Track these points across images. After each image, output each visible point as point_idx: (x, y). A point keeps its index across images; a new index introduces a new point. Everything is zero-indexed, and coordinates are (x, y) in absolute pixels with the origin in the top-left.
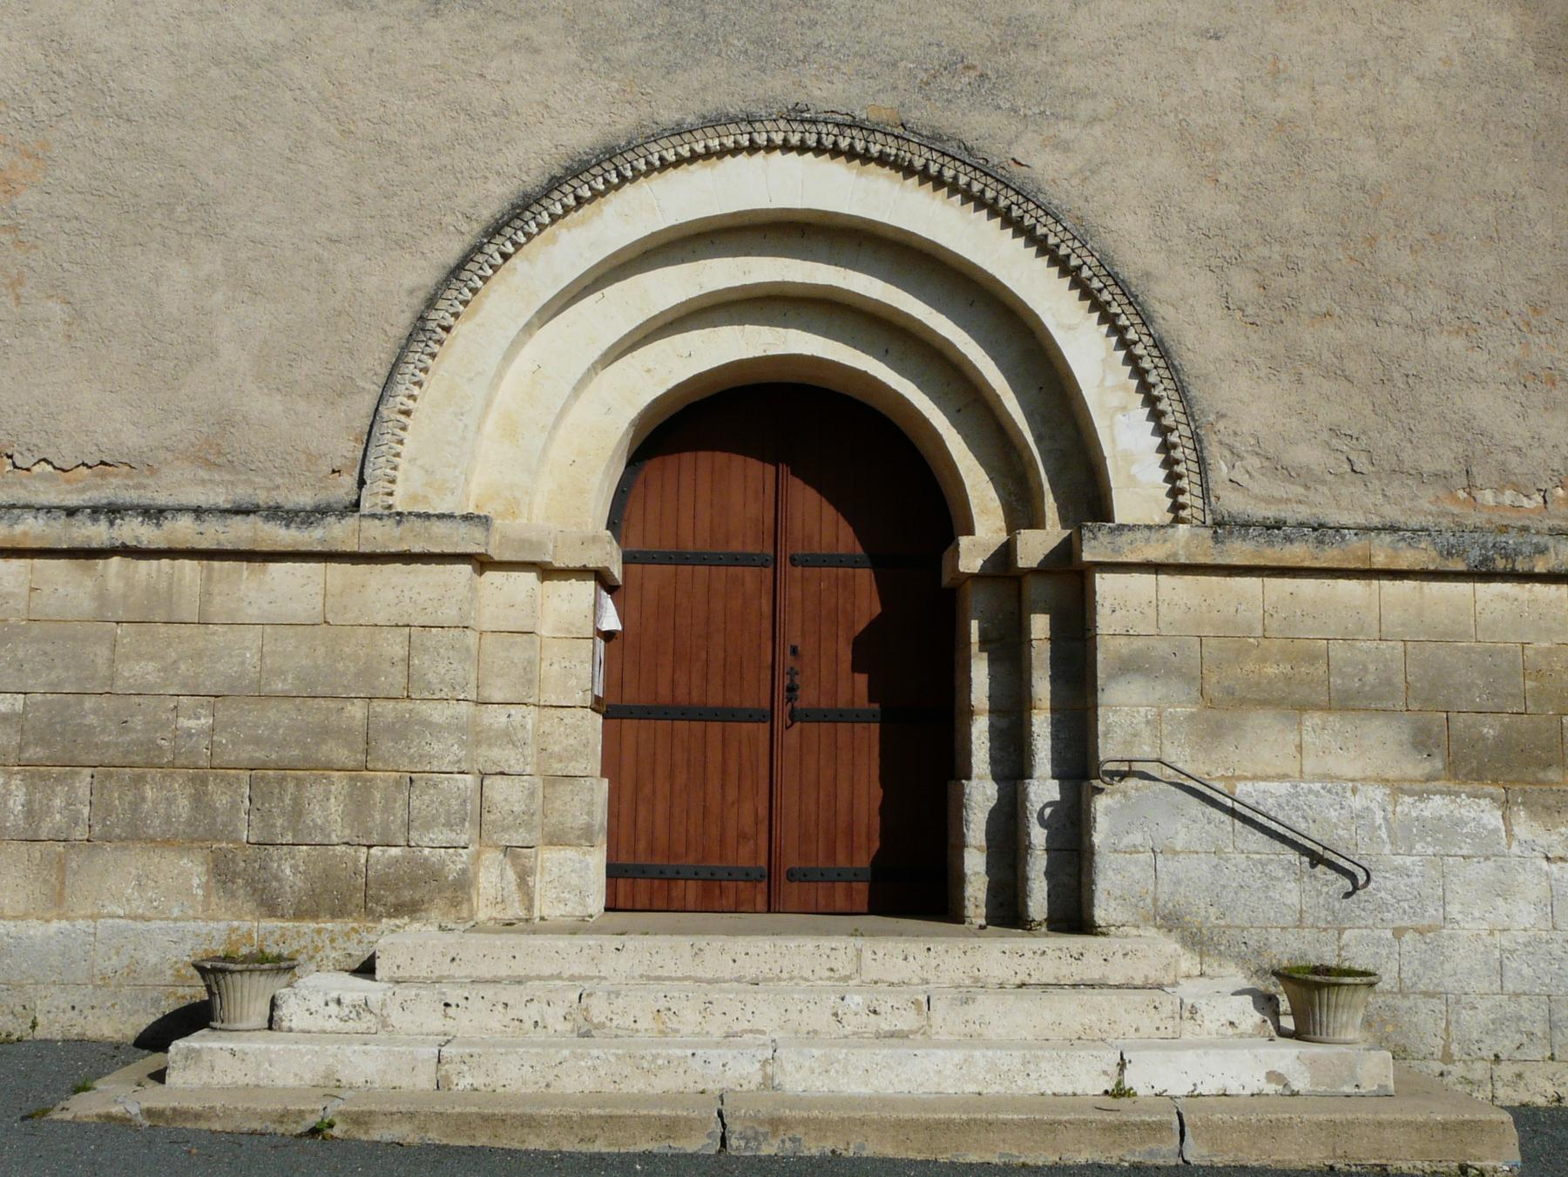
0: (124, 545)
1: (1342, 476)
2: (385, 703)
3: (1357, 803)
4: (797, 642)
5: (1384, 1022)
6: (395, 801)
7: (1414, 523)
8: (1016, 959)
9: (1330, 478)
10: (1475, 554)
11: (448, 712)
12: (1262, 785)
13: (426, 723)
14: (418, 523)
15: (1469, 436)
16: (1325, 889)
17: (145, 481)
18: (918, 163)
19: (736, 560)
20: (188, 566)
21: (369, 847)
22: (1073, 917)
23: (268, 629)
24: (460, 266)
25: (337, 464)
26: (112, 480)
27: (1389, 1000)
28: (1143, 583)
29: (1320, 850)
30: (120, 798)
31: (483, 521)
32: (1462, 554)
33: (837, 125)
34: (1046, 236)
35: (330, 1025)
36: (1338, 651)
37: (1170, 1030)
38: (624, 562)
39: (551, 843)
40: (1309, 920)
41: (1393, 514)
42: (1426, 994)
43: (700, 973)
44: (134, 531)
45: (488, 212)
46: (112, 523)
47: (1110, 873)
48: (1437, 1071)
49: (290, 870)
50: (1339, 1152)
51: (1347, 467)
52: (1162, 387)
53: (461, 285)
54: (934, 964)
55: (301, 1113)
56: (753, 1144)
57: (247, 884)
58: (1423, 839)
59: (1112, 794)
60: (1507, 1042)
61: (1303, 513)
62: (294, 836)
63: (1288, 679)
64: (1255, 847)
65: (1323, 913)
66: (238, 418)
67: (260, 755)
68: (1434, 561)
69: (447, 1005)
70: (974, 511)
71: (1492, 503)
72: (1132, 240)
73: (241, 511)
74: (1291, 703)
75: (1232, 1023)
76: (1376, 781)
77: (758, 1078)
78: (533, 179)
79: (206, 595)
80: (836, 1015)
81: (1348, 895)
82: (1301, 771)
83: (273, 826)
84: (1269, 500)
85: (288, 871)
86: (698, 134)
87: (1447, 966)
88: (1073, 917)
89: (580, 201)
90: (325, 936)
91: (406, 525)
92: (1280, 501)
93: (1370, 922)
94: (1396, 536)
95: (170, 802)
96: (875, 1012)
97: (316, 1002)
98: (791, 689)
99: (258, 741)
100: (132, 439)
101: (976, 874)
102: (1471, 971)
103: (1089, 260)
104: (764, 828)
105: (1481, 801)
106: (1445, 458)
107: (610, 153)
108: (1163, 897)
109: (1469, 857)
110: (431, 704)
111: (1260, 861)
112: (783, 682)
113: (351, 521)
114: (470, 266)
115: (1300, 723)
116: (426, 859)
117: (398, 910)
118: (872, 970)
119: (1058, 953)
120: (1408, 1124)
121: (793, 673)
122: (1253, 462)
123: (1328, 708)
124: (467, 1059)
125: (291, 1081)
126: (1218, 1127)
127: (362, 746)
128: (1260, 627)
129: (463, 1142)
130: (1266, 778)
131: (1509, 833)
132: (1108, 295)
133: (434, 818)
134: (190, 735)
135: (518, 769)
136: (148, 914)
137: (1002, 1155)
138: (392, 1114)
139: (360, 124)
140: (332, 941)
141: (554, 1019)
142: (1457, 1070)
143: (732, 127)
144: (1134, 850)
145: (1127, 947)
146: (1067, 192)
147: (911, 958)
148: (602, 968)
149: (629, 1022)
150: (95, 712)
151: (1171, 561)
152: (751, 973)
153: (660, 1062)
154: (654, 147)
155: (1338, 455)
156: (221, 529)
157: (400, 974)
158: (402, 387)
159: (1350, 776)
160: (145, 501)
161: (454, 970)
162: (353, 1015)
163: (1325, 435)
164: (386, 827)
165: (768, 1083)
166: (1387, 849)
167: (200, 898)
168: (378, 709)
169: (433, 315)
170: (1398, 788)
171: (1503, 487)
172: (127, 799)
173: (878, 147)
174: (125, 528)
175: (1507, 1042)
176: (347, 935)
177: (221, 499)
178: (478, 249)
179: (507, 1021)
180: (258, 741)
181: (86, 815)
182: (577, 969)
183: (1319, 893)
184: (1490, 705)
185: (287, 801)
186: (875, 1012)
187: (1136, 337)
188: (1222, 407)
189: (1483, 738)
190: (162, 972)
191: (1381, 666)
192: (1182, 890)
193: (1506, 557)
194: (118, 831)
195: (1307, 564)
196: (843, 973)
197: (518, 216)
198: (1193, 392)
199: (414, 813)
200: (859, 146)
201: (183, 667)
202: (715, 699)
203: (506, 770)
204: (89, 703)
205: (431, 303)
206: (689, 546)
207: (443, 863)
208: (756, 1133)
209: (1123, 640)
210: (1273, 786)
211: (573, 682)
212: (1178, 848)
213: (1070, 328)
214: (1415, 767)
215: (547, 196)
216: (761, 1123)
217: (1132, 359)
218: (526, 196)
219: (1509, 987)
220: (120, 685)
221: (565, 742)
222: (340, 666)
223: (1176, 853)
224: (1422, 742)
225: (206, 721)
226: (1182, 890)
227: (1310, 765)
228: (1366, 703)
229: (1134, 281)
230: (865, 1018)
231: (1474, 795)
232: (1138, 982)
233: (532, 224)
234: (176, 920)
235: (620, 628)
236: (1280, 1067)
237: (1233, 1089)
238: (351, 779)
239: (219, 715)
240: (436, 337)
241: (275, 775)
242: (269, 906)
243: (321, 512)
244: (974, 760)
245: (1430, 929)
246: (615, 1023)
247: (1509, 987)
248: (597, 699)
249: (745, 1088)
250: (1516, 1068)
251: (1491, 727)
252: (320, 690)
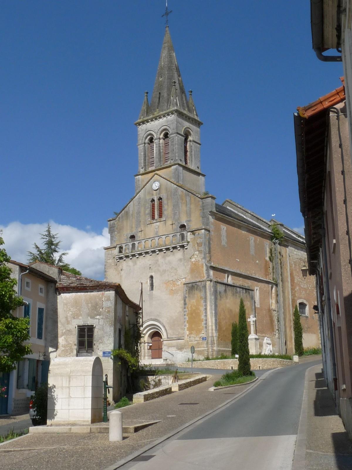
28: (165, 341)
106: (177, 333)
132: (164, 327)
170: (175, 351)
214: (176, 350)
224: (177, 348)
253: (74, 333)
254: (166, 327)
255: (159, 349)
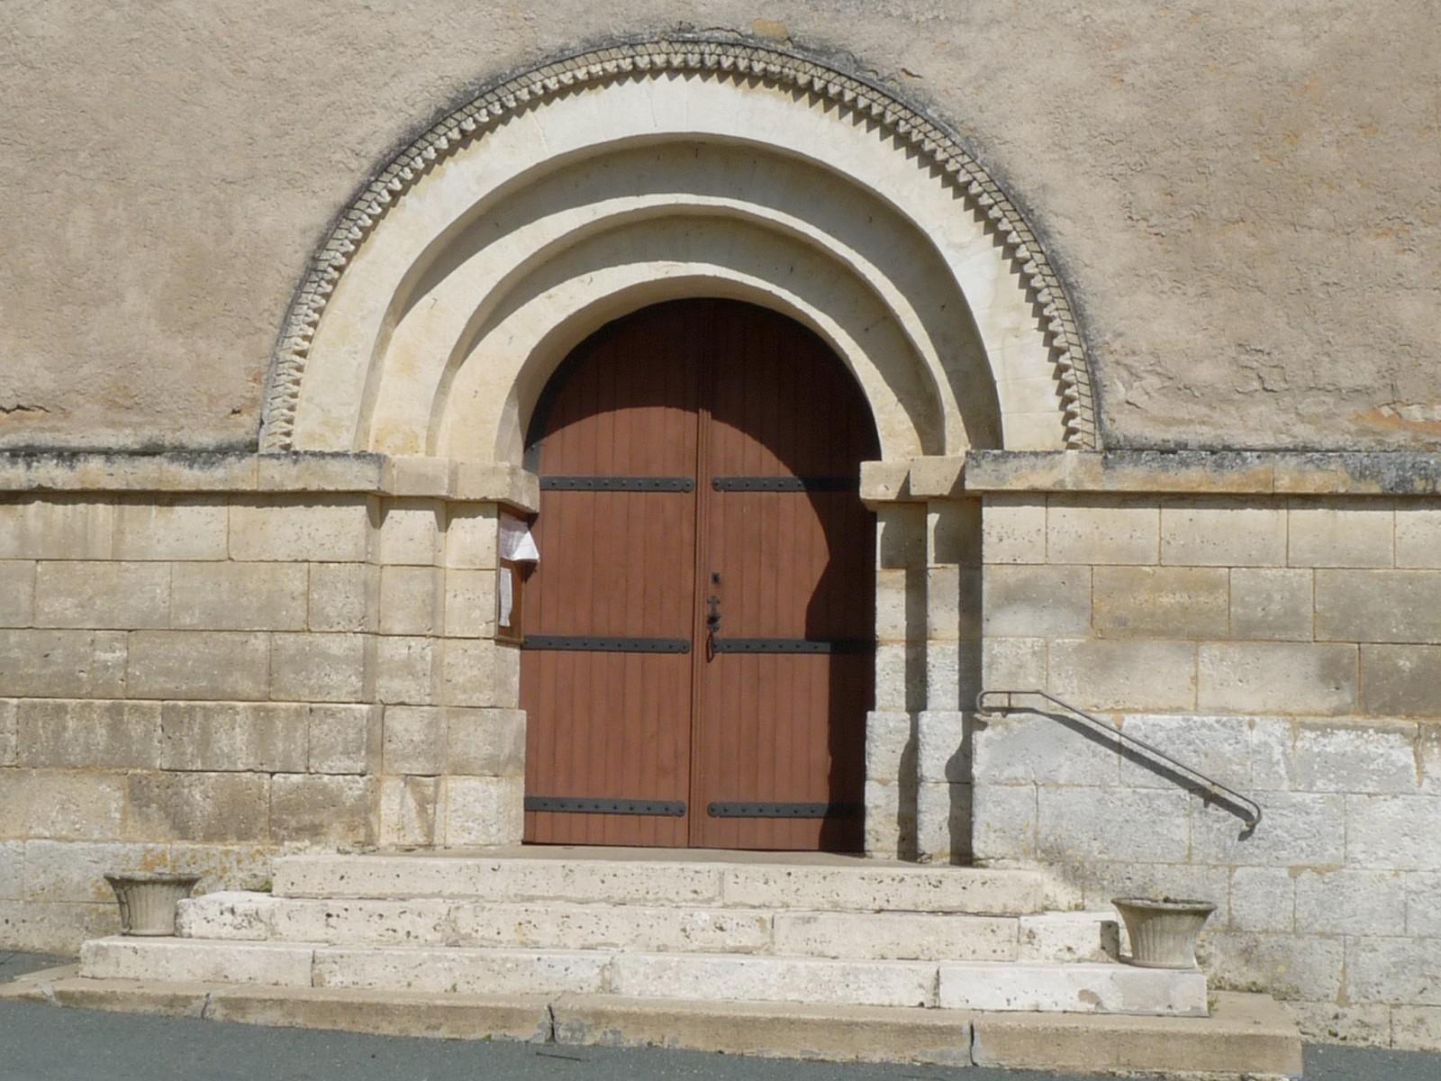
0: (40, 487)
1: (1250, 394)
2: (286, 635)
3: (1254, 737)
4: (718, 570)
5: (1275, 963)
6: (296, 729)
7: (1328, 443)
8: (875, 885)
9: (1237, 396)
10: (1391, 476)
11: (346, 645)
12: (1152, 718)
13: (325, 656)
14: (313, 462)
15: (1395, 347)
16: (1217, 826)
17: (60, 425)
18: (803, 79)
19: (656, 486)
20: (102, 510)
21: (272, 774)
22: (963, 855)
23: (176, 565)
24: (350, 206)
25: (237, 405)
26: (29, 423)
27: (1282, 940)
28: (1031, 515)
29: (1207, 784)
30: (44, 727)
31: (379, 460)
32: (1377, 476)
33: (720, 44)
34: (934, 151)
35: (225, 932)
36: (1240, 578)
37: (1007, 953)
38: (541, 490)
39: (455, 773)
40: (1196, 859)
41: (1304, 433)
42: (1322, 935)
43: (570, 893)
44: (51, 473)
45: (376, 148)
46: (29, 466)
47: (990, 805)
48: (1332, 1014)
49: (200, 797)
50: (1123, 1060)
51: (1256, 385)
52: (1053, 306)
53: (351, 224)
54: (794, 888)
55: (188, 999)
56: (578, 1035)
57: (160, 808)
58: (1324, 775)
59: (995, 725)
60: (1409, 986)
61: (1206, 434)
62: (203, 764)
63: (1184, 609)
64: (1142, 781)
65: (1214, 850)
66: (144, 360)
67: (171, 686)
68: (1344, 483)
69: (329, 915)
70: (881, 434)
71: (1421, 420)
72: (1029, 154)
73: (151, 451)
74: (1188, 632)
75: (1069, 949)
76: (1277, 714)
77: (597, 982)
78: (420, 113)
79: (119, 532)
80: (684, 930)
81: (1244, 836)
82: (1196, 704)
83: (184, 753)
84: (1170, 422)
85: (198, 797)
86: (580, 61)
87: (1346, 907)
88: (963, 855)
89: (395, 195)
90: (233, 858)
91: (302, 464)
92: (1181, 422)
93: (1264, 860)
94: (1303, 458)
95: (89, 730)
96: (721, 929)
97: (213, 911)
98: (712, 620)
99: (168, 673)
100: (46, 382)
101: (877, 807)
102: (1372, 912)
103: (979, 176)
104: (685, 760)
105: (1391, 737)
106: (1360, 370)
107: (493, 84)
108: (1044, 831)
109: (1375, 795)
110: (330, 637)
111: (1147, 795)
112: (704, 612)
113: (250, 461)
114: (360, 205)
115: (1196, 654)
116: (325, 786)
117: (300, 832)
118: (734, 893)
119: (917, 881)
120: (1191, 1036)
121: (714, 602)
122: (1153, 382)
123: (1226, 639)
124: (338, 959)
125: (186, 977)
126: (1006, 1033)
127: (265, 678)
128: (1156, 554)
129: (327, 1026)
130: (1159, 711)
131: (1421, 772)
132: (1003, 210)
133: (332, 747)
134: (107, 668)
135: (416, 700)
136: (72, 836)
137: (803, 1052)
138: (266, 1001)
139: (252, 62)
140: (239, 862)
141: (423, 927)
142: (1354, 1013)
143: (614, 52)
144: (1015, 782)
145: (1011, 878)
146: (960, 102)
147: (771, 883)
148: (480, 887)
149: (493, 934)
150: (20, 645)
151: (1058, 488)
152: (618, 895)
153: (509, 965)
154: (536, 76)
155: (1247, 372)
156: (129, 470)
157: (294, 890)
158: (299, 328)
159: (1250, 709)
160: (57, 444)
161: (342, 887)
162: (245, 924)
163: (1232, 352)
164: (287, 756)
165: (606, 987)
166: (1285, 786)
167: (118, 822)
168: (280, 642)
169: (325, 255)
170: (1298, 724)
171: (1432, 401)
172: (51, 728)
173: (762, 65)
174: (41, 470)
175: (1409, 986)
176: (253, 856)
177: (128, 439)
178: (367, 187)
179: (382, 931)
180: (168, 673)
181: (14, 743)
182: (455, 888)
183: (1210, 829)
184: (1407, 635)
185: (196, 730)
186: (721, 929)
187: (1027, 254)
188: (1120, 326)
189: (1399, 670)
190: (85, 890)
191: (1287, 594)
192: (1064, 823)
193: (1426, 478)
194: (43, 758)
195: (1203, 489)
196: (707, 895)
197: (403, 153)
198: (1090, 310)
199: (314, 741)
200: (742, 65)
201: (98, 602)
202: (635, 629)
203: (407, 701)
204: (14, 637)
205: (323, 244)
206: (609, 473)
207: (341, 790)
208: (582, 1025)
209: (1009, 570)
210: (1163, 719)
211: (476, 614)
212: (1061, 782)
213: (961, 247)
214: (1321, 700)
215: (431, 131)
216: (586, 1015)
217: (1026, 280)
218: (413, 130)
219: (1414, 929)
220: (41, 621)
221: (469, 674)
222: (244, 601)
223: (1059, 786)
224: (1332, 673)
225: (120, 654)
226: (1064, 823)
227: (1206, 698)
228: (1268, 634)
229: (1030, 194)
230: (712, 934)
231: (1385, 731)
232: (997, 910)
233: (419, 159)
234: (96, 841)
235: (536, 556)
236: (1093, 986)
237: (1046, 1004)
238: (255, 709)
239: (132, 648)
240: (327, 277)
241: (185, 710)
242: (184, 832)
243: (224, 451)
244: (878, 691)
245: (1329, 869)
246: (480, 934)
247: (1414, 929)
248: (501, 629)
249: (585, 990)
250: (1418, 1013)
251: (1408, 659)
252: (225, 625)
253: (983, 829)
254: (1067, 234)
255: (712, 647)
